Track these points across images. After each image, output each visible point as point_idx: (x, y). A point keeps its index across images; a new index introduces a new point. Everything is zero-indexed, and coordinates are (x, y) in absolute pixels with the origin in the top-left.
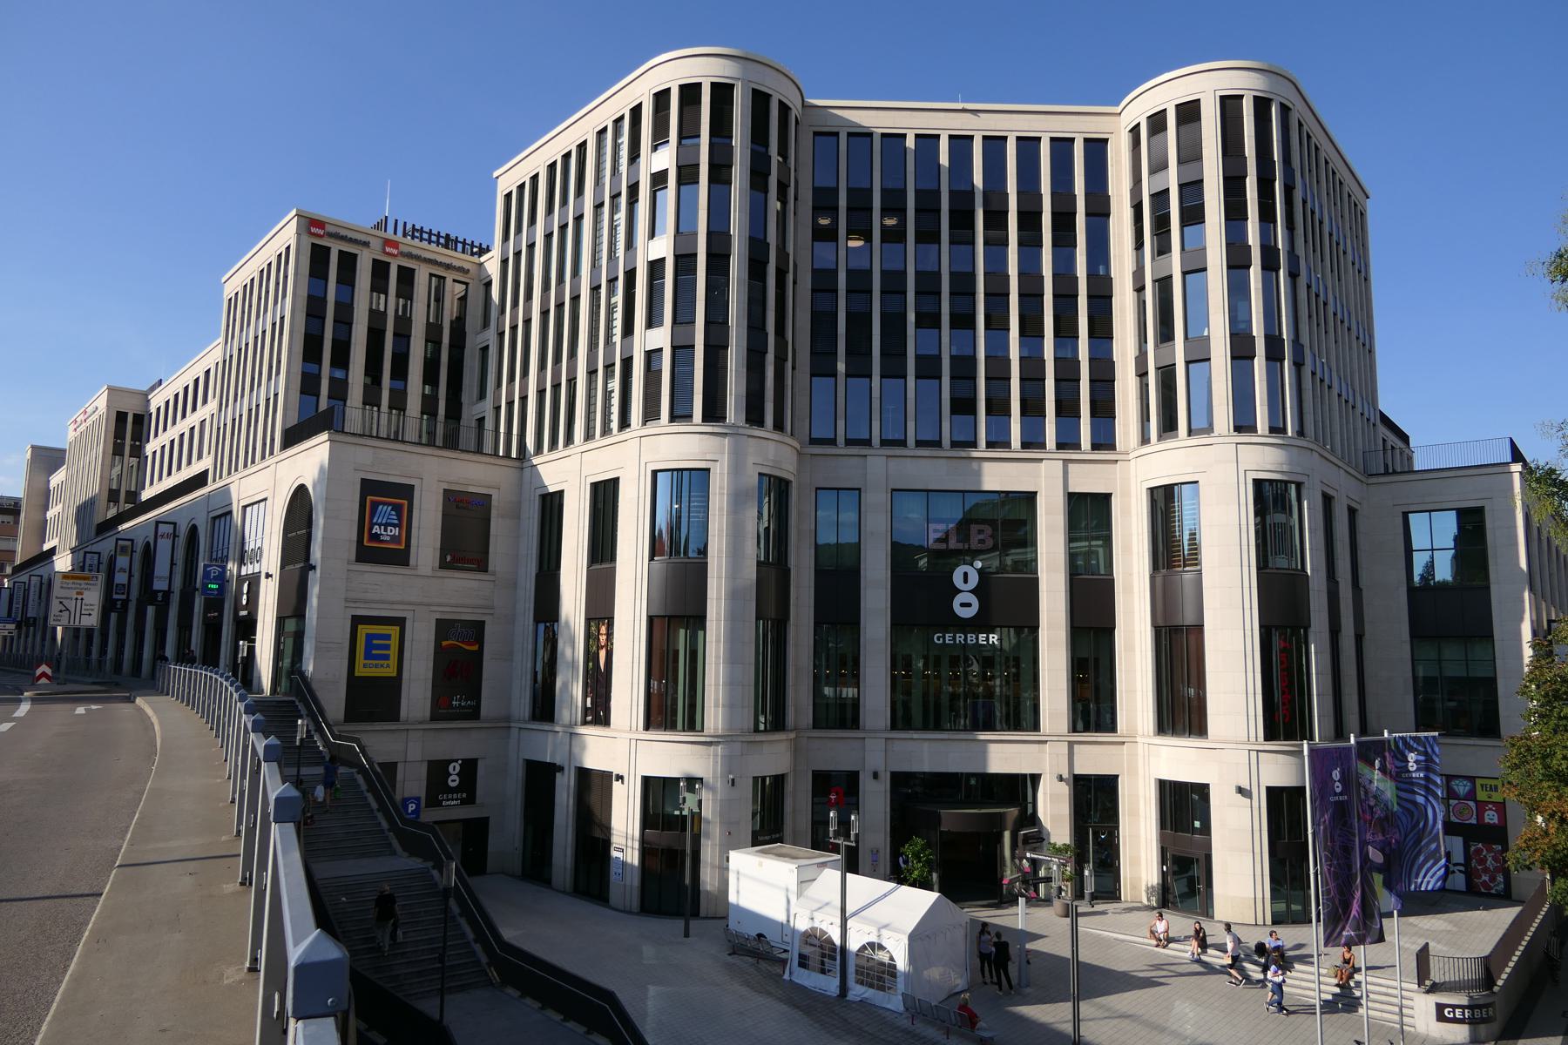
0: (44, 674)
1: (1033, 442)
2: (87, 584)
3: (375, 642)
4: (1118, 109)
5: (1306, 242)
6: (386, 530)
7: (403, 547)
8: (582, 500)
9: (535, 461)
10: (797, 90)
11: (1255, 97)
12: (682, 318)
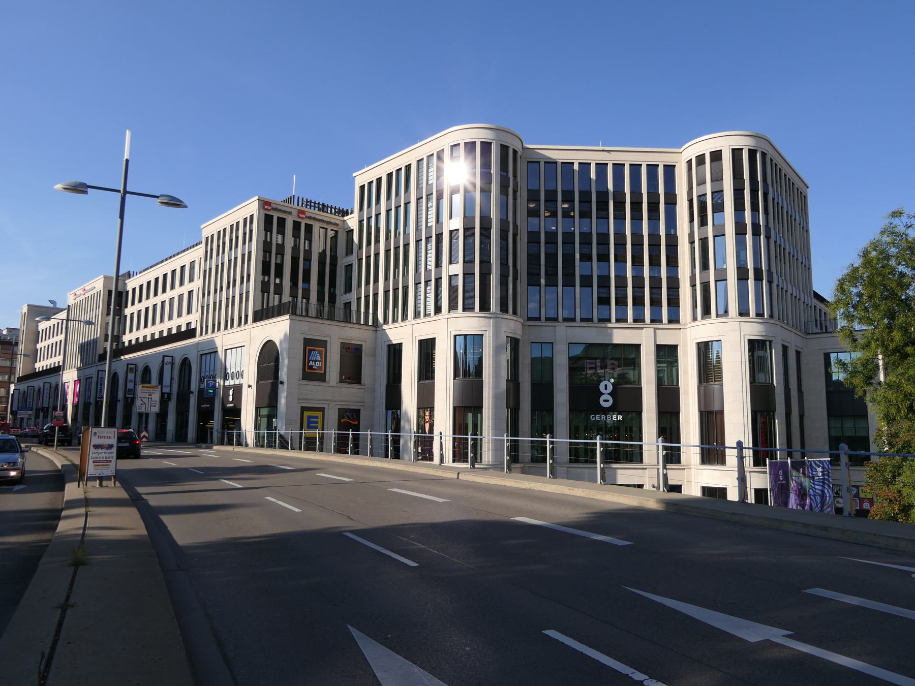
0: (144, 436)
1: (639, 319)
2: (153, 390)
3: (311, 420)
4: (681, 150)
5: (774, 219)
6: (315, 364)
7: (323, 372)
8: (414, 349)
9: (384, 327)
10: (520, 142)
11: (749, 149)
12: (468, 262)
